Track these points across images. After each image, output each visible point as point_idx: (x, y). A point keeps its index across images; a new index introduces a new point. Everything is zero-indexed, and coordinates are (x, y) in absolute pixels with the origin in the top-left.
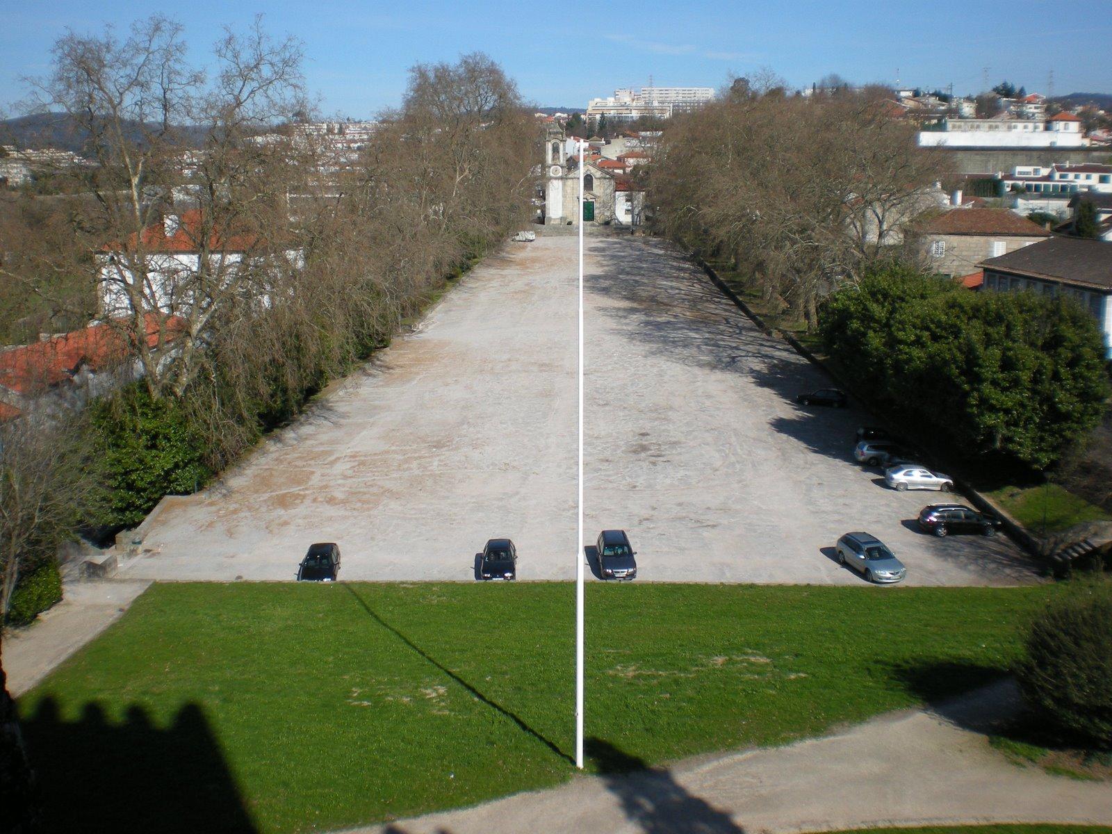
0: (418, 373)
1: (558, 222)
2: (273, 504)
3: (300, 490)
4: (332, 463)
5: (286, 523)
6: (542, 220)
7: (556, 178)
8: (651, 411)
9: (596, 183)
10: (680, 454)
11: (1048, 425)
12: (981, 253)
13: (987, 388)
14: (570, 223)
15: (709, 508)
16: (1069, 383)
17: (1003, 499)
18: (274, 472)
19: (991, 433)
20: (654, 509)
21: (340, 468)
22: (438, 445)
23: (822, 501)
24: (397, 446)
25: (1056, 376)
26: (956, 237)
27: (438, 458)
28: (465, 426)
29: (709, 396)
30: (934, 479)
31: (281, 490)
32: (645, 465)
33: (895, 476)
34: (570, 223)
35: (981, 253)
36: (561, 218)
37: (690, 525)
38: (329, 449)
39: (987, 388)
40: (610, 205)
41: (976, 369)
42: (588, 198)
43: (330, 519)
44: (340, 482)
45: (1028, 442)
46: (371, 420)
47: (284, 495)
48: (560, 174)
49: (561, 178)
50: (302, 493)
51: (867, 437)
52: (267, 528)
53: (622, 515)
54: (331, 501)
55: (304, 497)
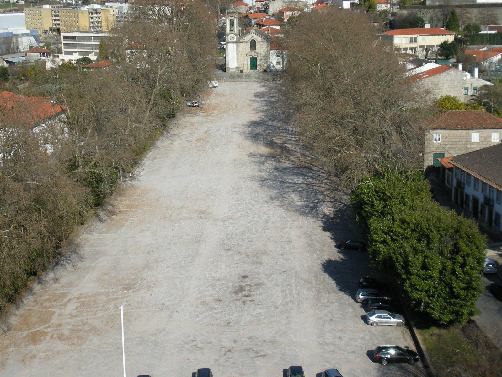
0: (127, 220)
1: (234, 70)
2: (28, 340)
3: (45, 328)
4: (66, 304)
5: (34, 357)
6: (223, 67)
7: (232, 42)
8: (253, 255)
9: (258, 45)
10: (260, 294)
11: (449, 299)
12: (464, 140)
13: (414, 279)
14: (242, 71)
15: (265, 341)
16: (462, 276)
17: (427, 337)
18: (32, 313)
19: (419, 302)
20: (235, 341)
21: (71, 308)
22: (128, 288)
23: (328, 334)
24: (105, 288)
25: (454, 272)
26: (447, 131)
27: (125, 300)
28: (146, 270)
29: (289, 242)
30: (393, 320)
31: (34, 328)
32: (239, 303)
33: (370, 318)
34: (242, 71)
35: (464, 140)
36: (236, 68)
37: (252, 355)
38: (66, 291)
39: (414, 279)
40: (267, 58)
41: (408, 267)
42: (253, 55)
43: (59, 353)
44: (69, 320)
45: (438, 308)
46: (93, 265)
47: (35, 333)
48: (235, 40)
49: (236, 42)
50: (46, 330)
51: (364, 287)
52: (23, 360)
53: (217, 347)
54: (61, 337)
55: (46, 333)
